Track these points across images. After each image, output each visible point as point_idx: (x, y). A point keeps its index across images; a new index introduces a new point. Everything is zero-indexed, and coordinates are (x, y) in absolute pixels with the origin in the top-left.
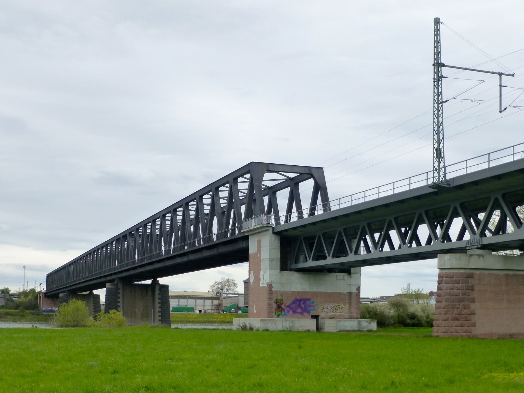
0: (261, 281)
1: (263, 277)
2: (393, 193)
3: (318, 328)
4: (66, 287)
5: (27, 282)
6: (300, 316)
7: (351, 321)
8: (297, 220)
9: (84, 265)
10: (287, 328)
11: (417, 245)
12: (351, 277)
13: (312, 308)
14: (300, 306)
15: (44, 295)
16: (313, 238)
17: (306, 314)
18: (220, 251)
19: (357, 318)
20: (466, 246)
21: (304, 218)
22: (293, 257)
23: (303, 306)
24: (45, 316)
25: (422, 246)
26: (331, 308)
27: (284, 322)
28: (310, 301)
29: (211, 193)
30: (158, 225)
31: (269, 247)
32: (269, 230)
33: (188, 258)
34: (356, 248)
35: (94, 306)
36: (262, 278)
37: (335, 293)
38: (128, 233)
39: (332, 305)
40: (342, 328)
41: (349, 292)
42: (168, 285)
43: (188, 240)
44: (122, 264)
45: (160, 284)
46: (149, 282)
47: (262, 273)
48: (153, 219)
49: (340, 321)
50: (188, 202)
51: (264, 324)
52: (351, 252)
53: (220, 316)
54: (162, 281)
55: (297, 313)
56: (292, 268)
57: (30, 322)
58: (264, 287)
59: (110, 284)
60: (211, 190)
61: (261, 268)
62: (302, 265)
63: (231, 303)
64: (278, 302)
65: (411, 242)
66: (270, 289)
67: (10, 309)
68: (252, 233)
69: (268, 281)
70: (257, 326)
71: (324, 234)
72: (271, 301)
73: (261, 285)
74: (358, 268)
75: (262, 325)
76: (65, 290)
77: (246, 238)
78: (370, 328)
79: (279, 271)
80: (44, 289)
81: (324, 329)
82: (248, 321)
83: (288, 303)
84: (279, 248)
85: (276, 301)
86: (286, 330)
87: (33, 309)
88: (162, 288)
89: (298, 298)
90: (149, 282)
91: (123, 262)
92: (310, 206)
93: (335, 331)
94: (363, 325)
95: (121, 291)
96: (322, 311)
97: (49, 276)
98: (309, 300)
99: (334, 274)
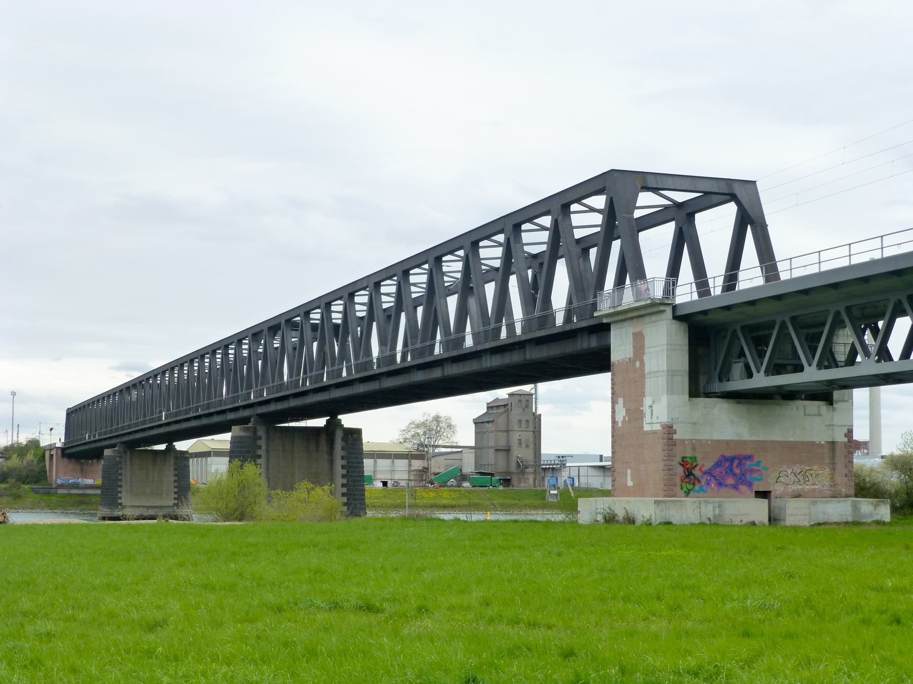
0: (647, 419)
1: (652, 411)
2: (880, 257)
3: (773, 519)
4: (117, 436)
5: (18, 425)
6: (732, 492)
7: (839, 502)
8: (763, 284)
9: (164, 389)
10: (709, 519)
12: (834, 410)
13: (755, 475)
14: (731, 470)
15: (60, 452)
16: (770, 325)
17: (743, 488)
18: (528, 357)
19: (847, 496)
21: (782, 279)
22: (715, 369)
23: (737, 471)
24: (64, 496)
26: (796, 475)
27: (703, 506)
28: (752, 461)
29: (395, 278)
30: (167, 377)
31: (665, 347)
32: (665, 310)
33: (443, 371)
35: (175, 475)
36: (647, 411)
37: (802, 443)
38: (283, 322)
39: (797, 469)
40: (821, 519)
41: (831, 440)
42: (361, 429)
43: (271, 382)
44: (236, 394)
45: (345, 426)
46: (320, 422)
47: (647, 401)
48: (326, 301)
49: (816, 502)
50: (568, 202)
51: (663, 511)
53: (427, 493)
54: (348, 420)
55: (726, 485)
56: (709, 391)
57: (33, 509)
58: (654, 432)
59: (240, 429)
60: (503, 229)
61: (644, 392)
62: (739, 384)
63: (447, 466)
64: (687, 463)
66: (670, 436)
68: (616, 318)
69: (664, 419)
70: (647, 516)
71: (793, 319)
72: (672, 461)
73: (647, 428)
74: (846, 391)
75: (657, 513)
76: (114, 441)
77: (602, 329)
78: (879, 518)
79: (686, 396)
80: (60, 440)
81: (785, 520)
82: (620, 506)
83: (708, 465)
84: (686, 348)
85: (683, 461)
86: (708, 522)
87: (36, 482)
88: (350, 436)
89: (729, 453)
90: (320, 422)
91: (240, 390)
92: (726, 272)
93: (807, 524)
94: (862, 511)
95: (262, 443)
96: (777, 482)
97: (72, 413)
98: (750, 458)
99: (799, 403)
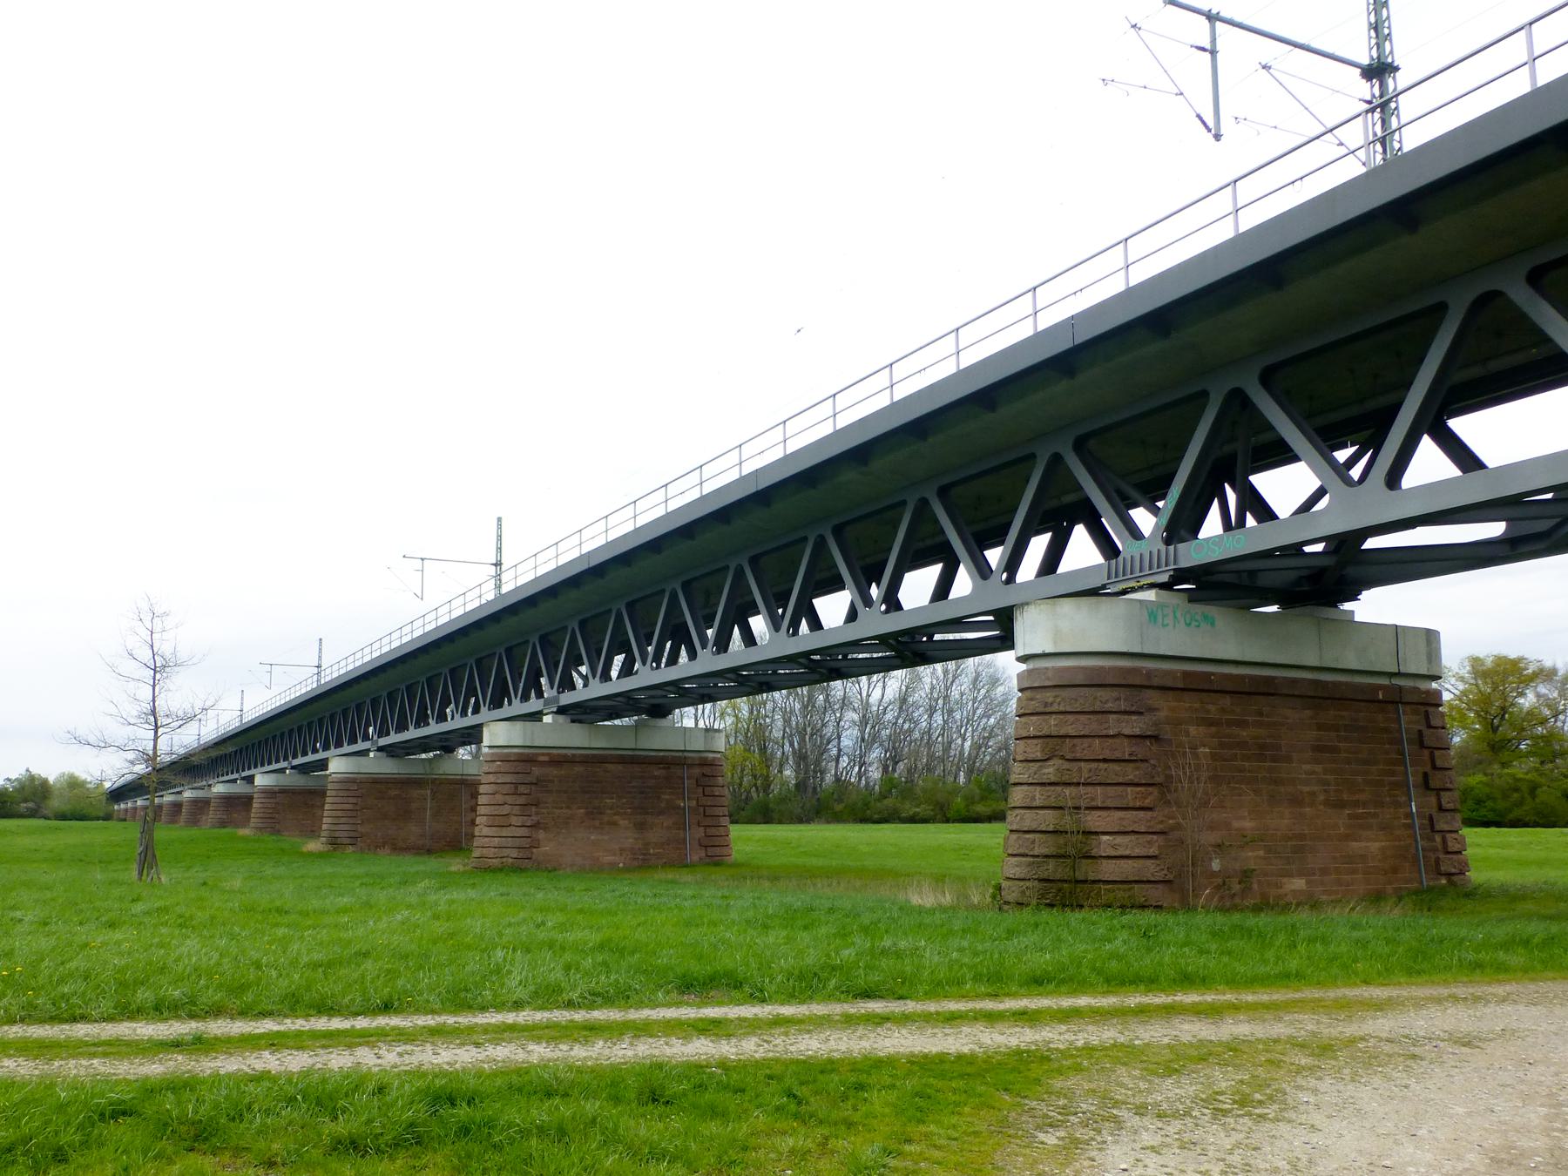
11: (1462, 471)
20: (542, 708)
25: (905, 608)
34: (792, 615)
52: (516, 698)
65: (795, 625)
67: (518, 1005)
